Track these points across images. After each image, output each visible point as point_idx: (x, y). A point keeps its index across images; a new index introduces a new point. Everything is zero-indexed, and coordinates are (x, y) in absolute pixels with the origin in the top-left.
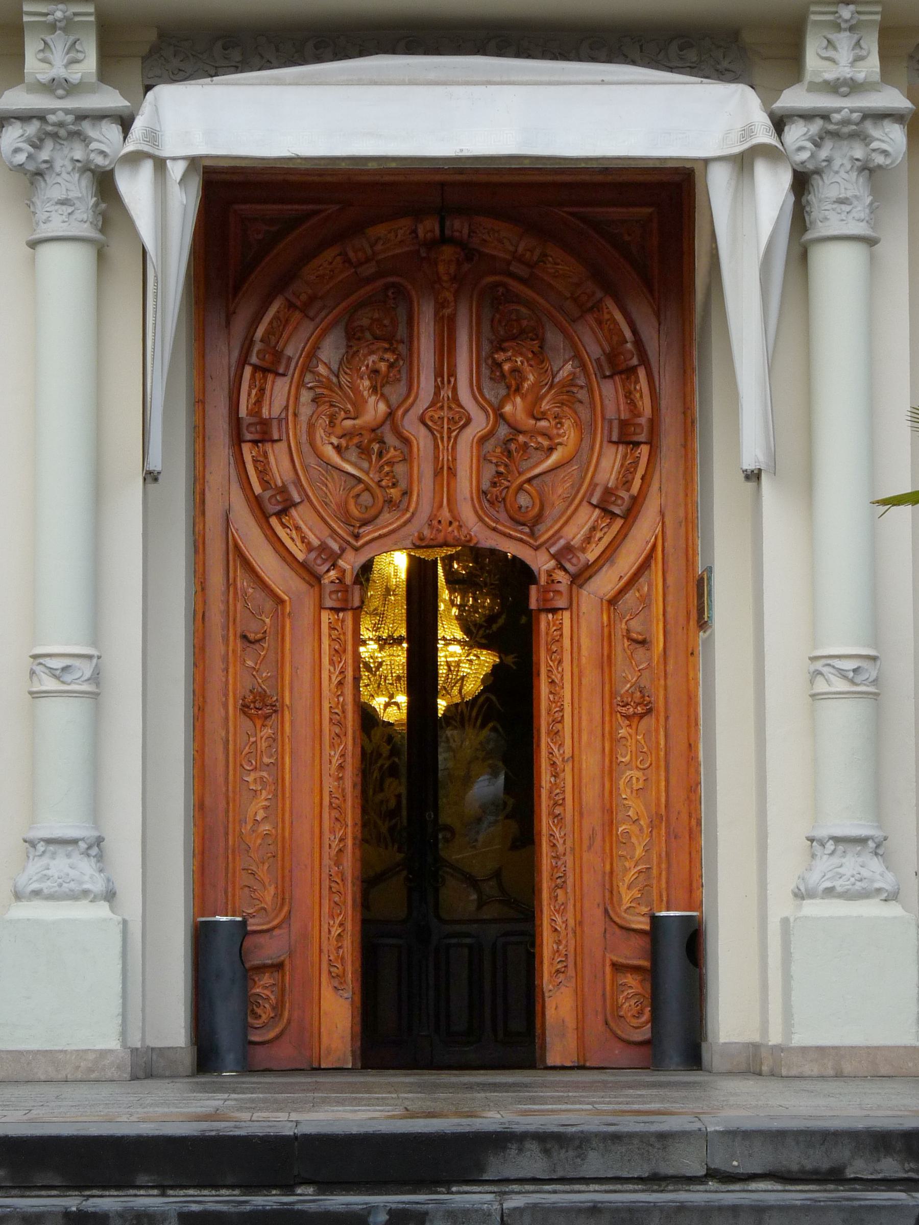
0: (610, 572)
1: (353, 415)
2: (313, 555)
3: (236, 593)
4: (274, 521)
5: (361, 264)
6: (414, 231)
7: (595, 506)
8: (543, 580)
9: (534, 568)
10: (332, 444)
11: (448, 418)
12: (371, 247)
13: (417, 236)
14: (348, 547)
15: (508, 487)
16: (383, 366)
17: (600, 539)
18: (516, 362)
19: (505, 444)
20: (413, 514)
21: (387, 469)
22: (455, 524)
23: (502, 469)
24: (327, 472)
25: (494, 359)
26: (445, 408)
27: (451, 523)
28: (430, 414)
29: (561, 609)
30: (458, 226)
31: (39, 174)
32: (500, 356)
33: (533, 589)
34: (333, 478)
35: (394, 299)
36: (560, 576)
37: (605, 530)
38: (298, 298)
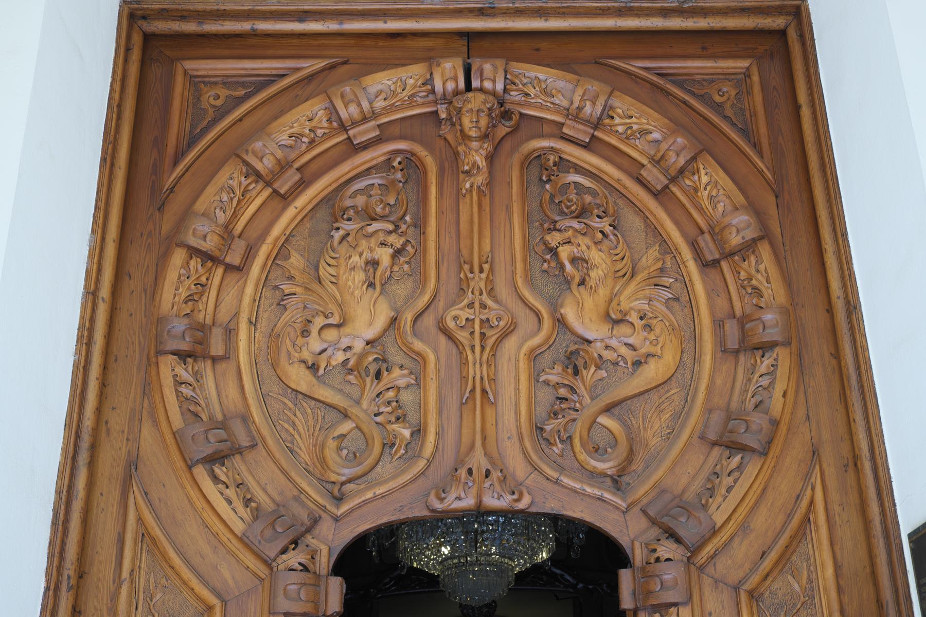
0: (808, 437)
1: (334, 320)
2: (259, 526)
3: (133, 593)
4: (200, 472)
5: (355, 124)
6: (429, 81)
7: (715, 444)
8: (638, 556)
9: (624, 541)
10: (304, 362)
11: (481, 320)
12: (370, 103)
13: (433, 91)
14: (324, 515)
15: (574, 420)
16: (384, 255)
17: (729, 490)
18: (549, 160)
19: (569, 358)
20: (430, 462)
21: (391, 394)
22: (496, 474)
23: (563, 392)
24: (295, 405)
25: (546, 244)
26: (477, 305)
27: (488, 474)
28: (453, 313)
29: (675, 605)
30: (491, 74)
31: (419, 430)
32: (554, 239)
33: (625, 577)
34: (304, 413)
35: (402, 170)
36: (666, 549)
37: (736, 474)
38: (261, 159)
